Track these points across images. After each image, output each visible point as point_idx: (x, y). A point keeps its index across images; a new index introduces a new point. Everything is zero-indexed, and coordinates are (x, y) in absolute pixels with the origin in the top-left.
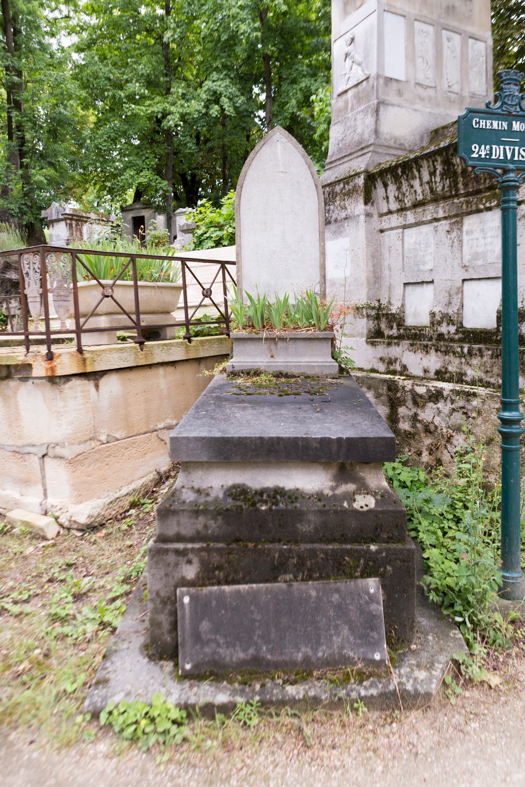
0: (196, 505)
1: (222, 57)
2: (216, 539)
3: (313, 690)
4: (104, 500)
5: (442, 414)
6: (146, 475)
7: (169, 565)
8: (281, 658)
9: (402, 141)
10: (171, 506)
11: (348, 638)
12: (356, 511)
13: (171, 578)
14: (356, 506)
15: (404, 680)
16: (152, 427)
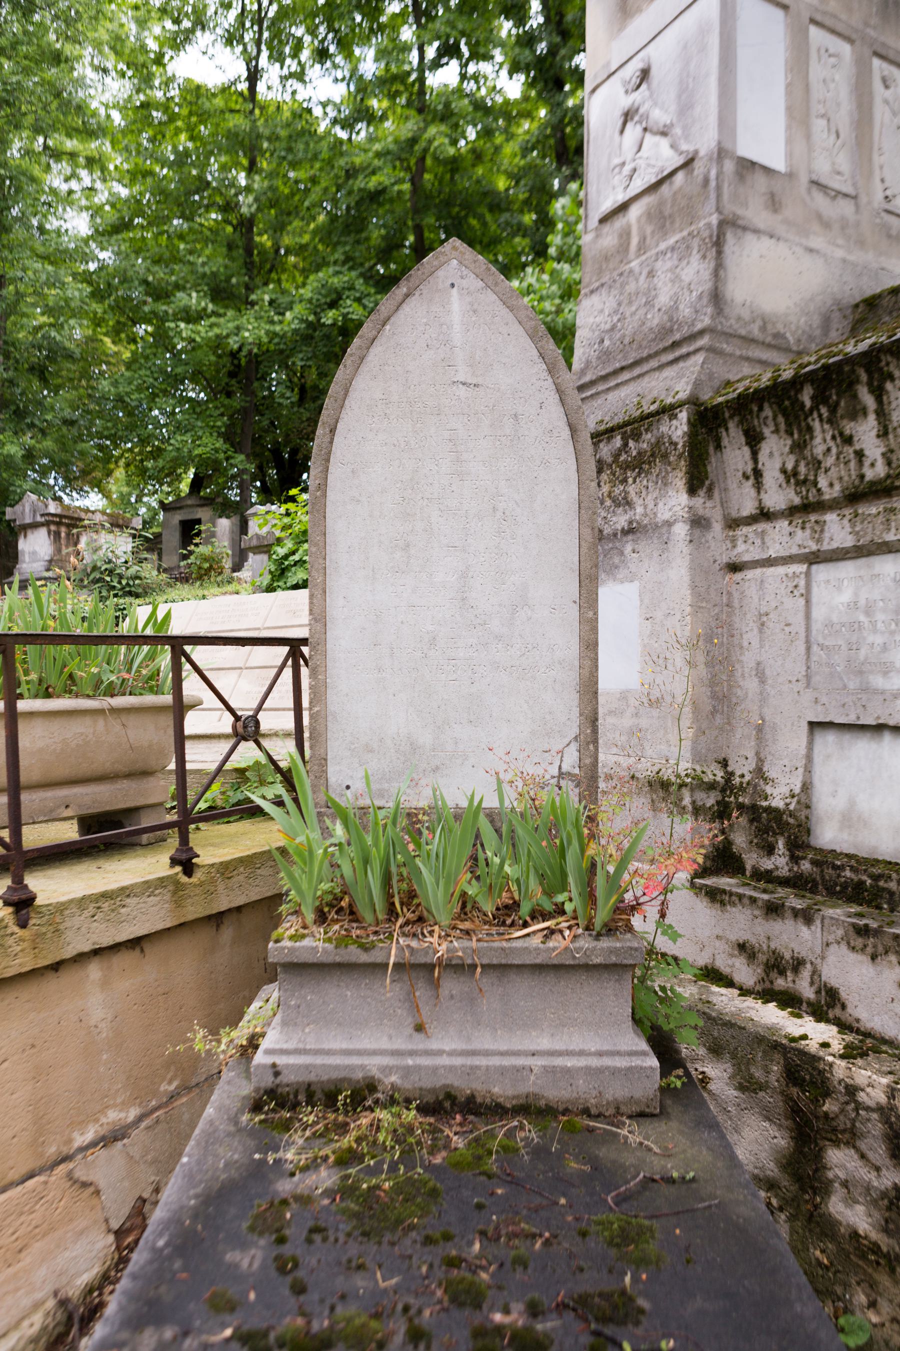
1: (345, 243)
6: (17, 1325)
9: (780, 327)
16: (52, 1151)
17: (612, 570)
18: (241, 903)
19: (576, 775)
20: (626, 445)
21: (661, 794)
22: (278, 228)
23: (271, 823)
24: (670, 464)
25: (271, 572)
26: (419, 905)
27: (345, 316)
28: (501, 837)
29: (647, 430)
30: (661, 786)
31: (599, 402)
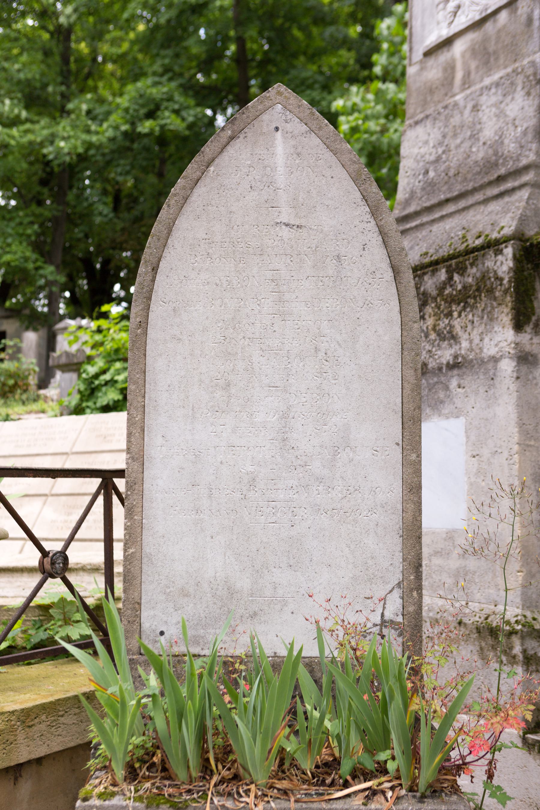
1: (164, 57)
17: (437, 406)
18: (42, 754)
19: (400, 623)
20: (451, 278)
21: (490, 641)
22: (96, 36)
23: (75, 665)
24: (495, 299)
25: (80, 392)
26: (235, 761)
27: (162, 127)
28: (320, 688)
29: (472, 265)
30: (490, 634)
31: (424, 233)
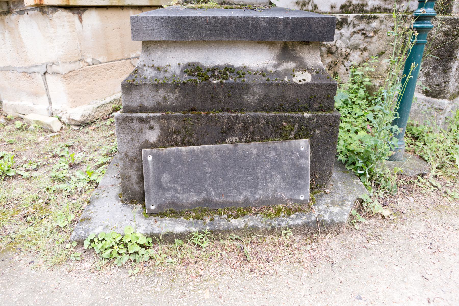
0: (156, 80)
2: (174, 109)
3: (251, 221)
4: (93, 105)
5: (343, 38)
7: (134, 131)
8: (226, 200)
10: (134, 80)
11: (280, 184)
12: (295, 84)
13: (136, 141)
14: (295, 80)
15: (322, 213)
16: (126, 56)
